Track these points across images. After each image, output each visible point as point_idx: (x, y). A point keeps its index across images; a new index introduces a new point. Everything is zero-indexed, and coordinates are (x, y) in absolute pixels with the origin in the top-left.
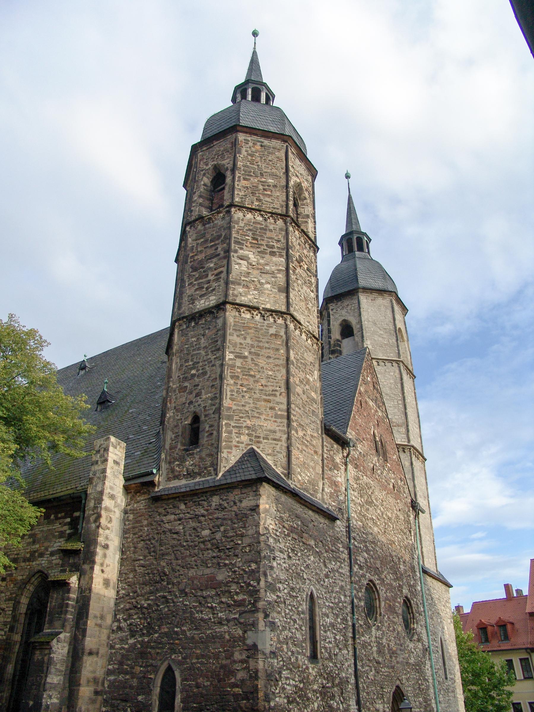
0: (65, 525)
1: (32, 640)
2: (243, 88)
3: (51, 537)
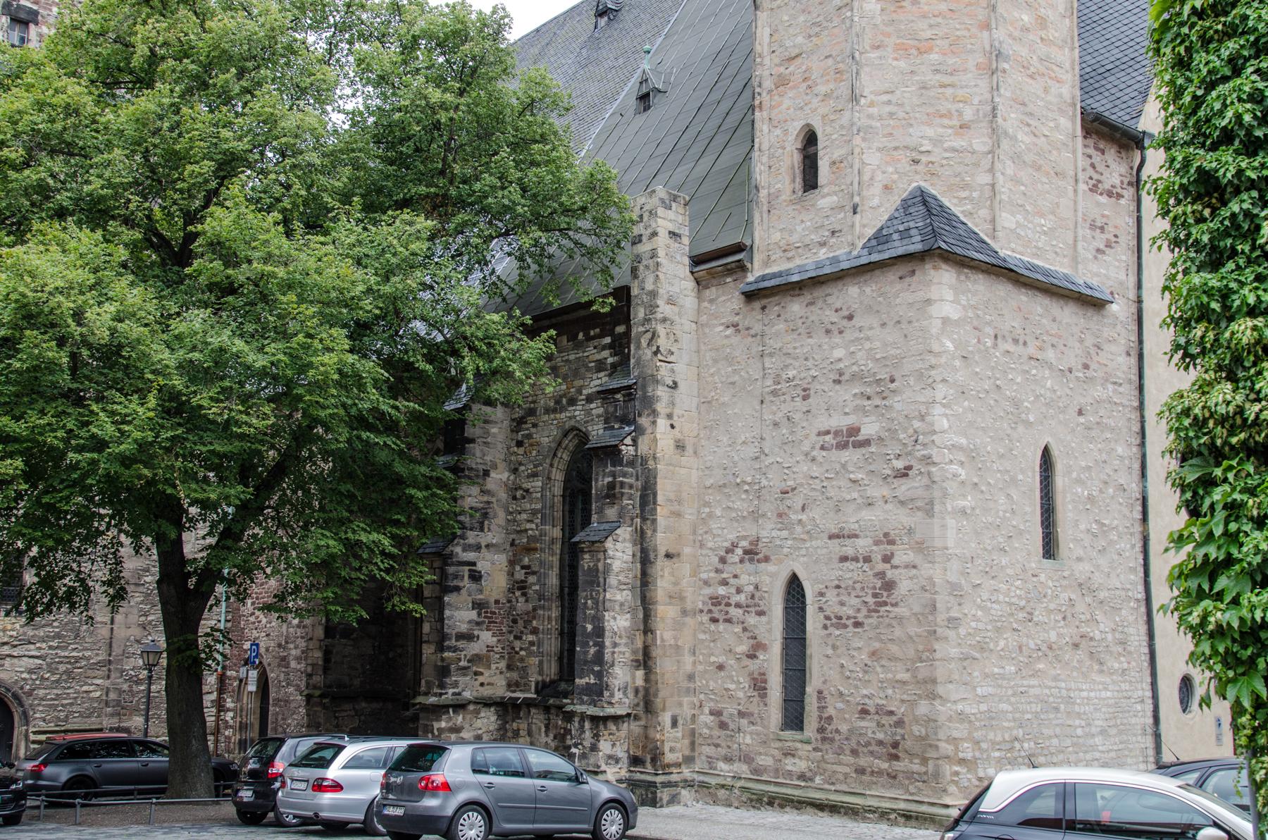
0: (604, 348)
1: (576, 539)
3: (583, 370)
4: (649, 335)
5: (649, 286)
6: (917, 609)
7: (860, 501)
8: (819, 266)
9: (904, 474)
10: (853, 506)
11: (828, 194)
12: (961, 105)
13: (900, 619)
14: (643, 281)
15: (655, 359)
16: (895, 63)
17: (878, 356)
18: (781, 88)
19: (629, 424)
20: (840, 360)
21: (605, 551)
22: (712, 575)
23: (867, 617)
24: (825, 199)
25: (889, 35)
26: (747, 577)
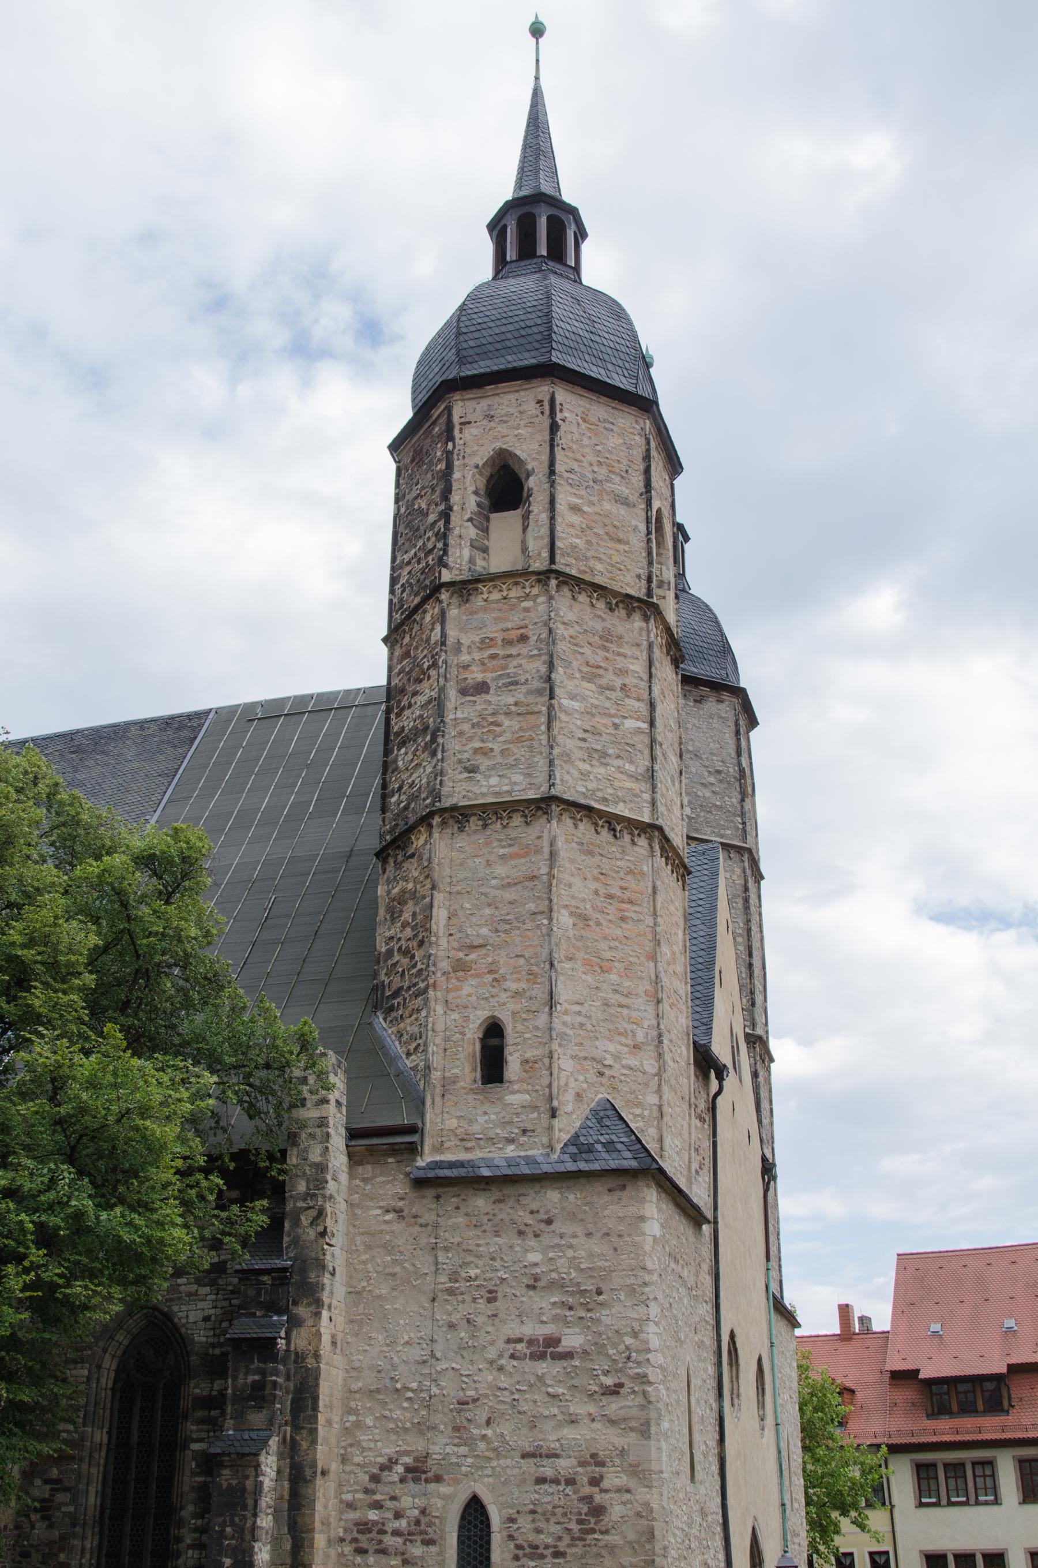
2: (526, 209)
4: (313, 1213)
5: (315, 1156)
6: (631, 1536)
7: (560, 1417)
8: (510, 1162)
9: (615, 1391)
10: (552, 1423)
11: (518, 1091)
12: (635, 1027)
13: (611, 1548)
14: (306, 1150)
15: (321, 1241)
16: (584, 977)
17: (583, 1266)
18: (461, 973)
19: (279, 1313)
20: (536, 1264)
21: (259, 1465)
22: (360, 1496)
23: (569, 1546)
24: (516, 1094)
25: (578, 950)
26: (409, 1502)
